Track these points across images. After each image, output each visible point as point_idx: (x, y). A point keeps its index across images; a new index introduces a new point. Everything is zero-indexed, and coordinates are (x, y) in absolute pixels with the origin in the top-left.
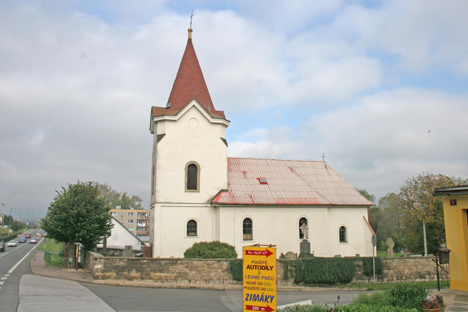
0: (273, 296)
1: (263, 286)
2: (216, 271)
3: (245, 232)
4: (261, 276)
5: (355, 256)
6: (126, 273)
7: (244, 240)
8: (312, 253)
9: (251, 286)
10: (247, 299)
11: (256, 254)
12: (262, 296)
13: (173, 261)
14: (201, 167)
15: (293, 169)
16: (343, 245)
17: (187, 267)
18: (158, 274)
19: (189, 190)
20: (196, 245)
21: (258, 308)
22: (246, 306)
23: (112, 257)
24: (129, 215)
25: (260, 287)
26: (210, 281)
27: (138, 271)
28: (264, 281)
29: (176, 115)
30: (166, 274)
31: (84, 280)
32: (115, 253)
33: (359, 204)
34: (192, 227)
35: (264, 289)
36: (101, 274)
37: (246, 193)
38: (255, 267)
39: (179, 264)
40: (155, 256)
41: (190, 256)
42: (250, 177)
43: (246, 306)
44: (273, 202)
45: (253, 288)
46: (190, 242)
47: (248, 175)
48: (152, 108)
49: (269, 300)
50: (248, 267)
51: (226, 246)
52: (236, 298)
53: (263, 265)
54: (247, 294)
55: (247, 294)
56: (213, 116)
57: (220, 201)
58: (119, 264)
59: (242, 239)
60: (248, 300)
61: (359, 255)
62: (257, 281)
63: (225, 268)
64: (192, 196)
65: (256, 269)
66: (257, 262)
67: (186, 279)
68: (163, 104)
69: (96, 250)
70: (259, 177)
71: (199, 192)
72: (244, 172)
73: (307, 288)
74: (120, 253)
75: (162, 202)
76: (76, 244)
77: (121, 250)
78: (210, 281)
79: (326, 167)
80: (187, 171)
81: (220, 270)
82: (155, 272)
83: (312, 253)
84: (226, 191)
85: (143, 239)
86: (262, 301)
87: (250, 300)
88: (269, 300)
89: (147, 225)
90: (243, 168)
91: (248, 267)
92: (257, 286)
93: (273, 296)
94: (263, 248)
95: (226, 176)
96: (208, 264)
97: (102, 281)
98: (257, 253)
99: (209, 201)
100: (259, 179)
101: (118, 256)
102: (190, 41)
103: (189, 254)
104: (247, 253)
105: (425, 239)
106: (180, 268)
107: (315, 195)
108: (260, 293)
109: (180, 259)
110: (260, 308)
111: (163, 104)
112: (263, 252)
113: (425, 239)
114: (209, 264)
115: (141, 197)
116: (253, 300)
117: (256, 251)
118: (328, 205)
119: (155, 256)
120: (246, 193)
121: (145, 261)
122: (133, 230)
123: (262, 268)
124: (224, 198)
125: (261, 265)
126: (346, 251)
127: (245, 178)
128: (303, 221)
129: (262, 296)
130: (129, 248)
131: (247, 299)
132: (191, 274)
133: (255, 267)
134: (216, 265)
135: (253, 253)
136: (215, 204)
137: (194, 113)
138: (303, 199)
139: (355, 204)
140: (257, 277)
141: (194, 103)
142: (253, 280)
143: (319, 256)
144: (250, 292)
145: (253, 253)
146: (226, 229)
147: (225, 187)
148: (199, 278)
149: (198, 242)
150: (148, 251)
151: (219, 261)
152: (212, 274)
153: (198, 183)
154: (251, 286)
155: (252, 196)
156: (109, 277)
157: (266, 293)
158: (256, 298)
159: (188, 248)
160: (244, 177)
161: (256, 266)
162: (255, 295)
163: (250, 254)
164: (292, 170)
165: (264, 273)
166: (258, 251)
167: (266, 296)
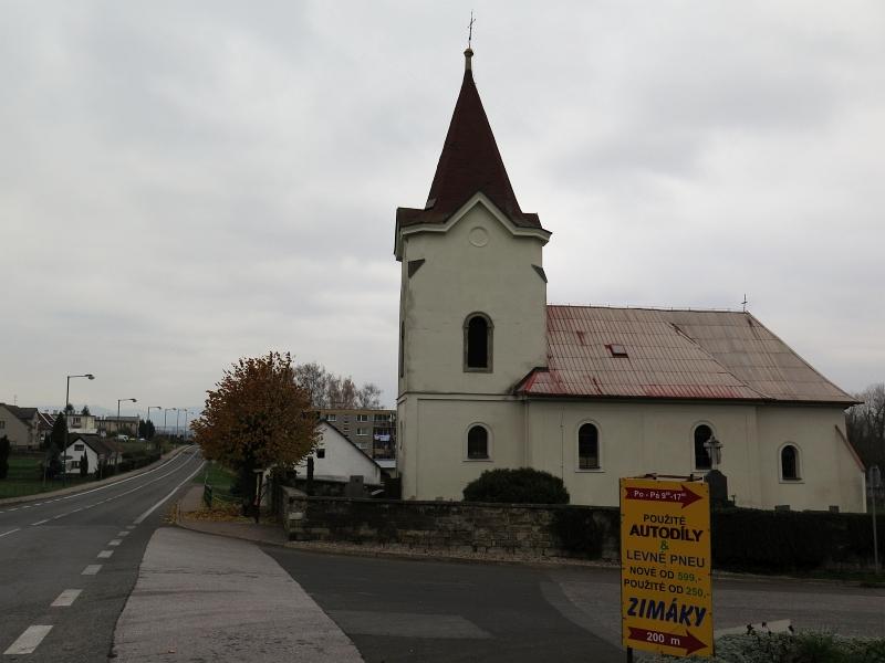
0: (704, 610)
1: (676, 582)
2: (527, 529)
3: (583, 452)
4: (668, 553)
5: (828, 509)
6: (349, 530)
7: (581, 467)
8: (730, 498)
9: (642, 578)
10: (631, 613)
11: (654, 498)
12: (674, 606)
13: (441, 508)
17: (470, 520)
18: (412, 532)
20: (486, 475)
21: (661, 638)
22: (631, 629)
23: (324, 498)
24: (359, 419)
25: (667, 582)
26: (516, 549)
27: (371, 526)
28: (676, 567)
29: (445, 222)
30: (427, 533)
31: (270, 542)
32: (333, 490)
34: (478, 441)
35: (678, 589)
36: (300, 530)
37: (585, 374)
38: (651, 530)
39: (454, 513)
40: (406, 496)
41: (649, 484)
42: (592, 344)
43: (631, 629)
44: (639, 392)
45: (647, 585)
46: (475, 471)
47: (588, 339)
48: (399, 210)
49: (693, 617)
50: (634, 530)
51: (546, 477)
52: (590, 601)
53: (674, 526)
54: (632, 600)
55: (632, 600)
56: (517, 222)
57: (535, 388)
58: (335, 511)
60: (634, 614)
61: (837, 508)
62: (659, 566)
63: (547, 523)
65: (655, 535)
66: (657, 519)
67: (467, 543)
68: (419, 200)
69: (294, 484)
71: (491, 371)
72: (580, 334)
73: (723, 573)
74: (341, 489)
76: (256, 471)
77: (342, 485)
78: (516, 549)
79: (750, 322)
81: (536, 529)
82: (407, 528)
83: (730, 498)
84: (545, 370)
85: (384, 464)
86: (672, 619)
87: (641, 615)
88: (693, 617)
89: (391, 438)
90: (577, 326)
91: (634, 530)
92: (658, 579)
93: (704, 610)
94: (676, 484)
95: (544, 341)
96: (512, 515)
97: (302, 545)
98: (658, 496)
99: (511, 389)
100: (609, 347)
101: (336, 495)
103: (476, 492)
104: (630, 493)
105: (153, 509)
106: (456, 520)
107: (727, 379)
108: (666, 597)
109: (455, 504)
110: (668, 637)
111: (419, 200)
112: (673, 492)
113: (153, 509)
114: (514, 514)
115: (378, 386)
116: (648, 616)
117: (655, 491)
118: (758, 400)
119: (406, 496)
120: (585, 374)
121: (387, 506)
122: (368, 447)
123: (670, 534)
124: (541, 385)
125: (669, 527)
126: (798, 499)
127: (582, 345)
128: (703, 434)
129: (674, 606)
130: (357, 479)
131: (631, 613)
132: (477, 533)
133: (651, 530)
134: (528, 517)
135: (646, 494)
136: (521, 394)
137: (479, 219)
139: (814, 399)
140: (658, 558)
141: (479, 198)
142: (648, 565)
144: (640, 594)
145: (646, 494)
146: (547, 447)
147: (542, 364)
148: (494, 543)
149: (491, 470)
150: (392, 483)
151: (534, 509)
152: (521, 536)
153: (488, 354)
154: (642, 578)
156: (315, 538)
157: (683, 600)
158: (655, 610)
159: (472, 480)
161: (655, 528)
162: (652, 603)
163: (638, 497)
164: (677, 329)
165: (677, 547)
166: (660, 492)
167: (684, 607)
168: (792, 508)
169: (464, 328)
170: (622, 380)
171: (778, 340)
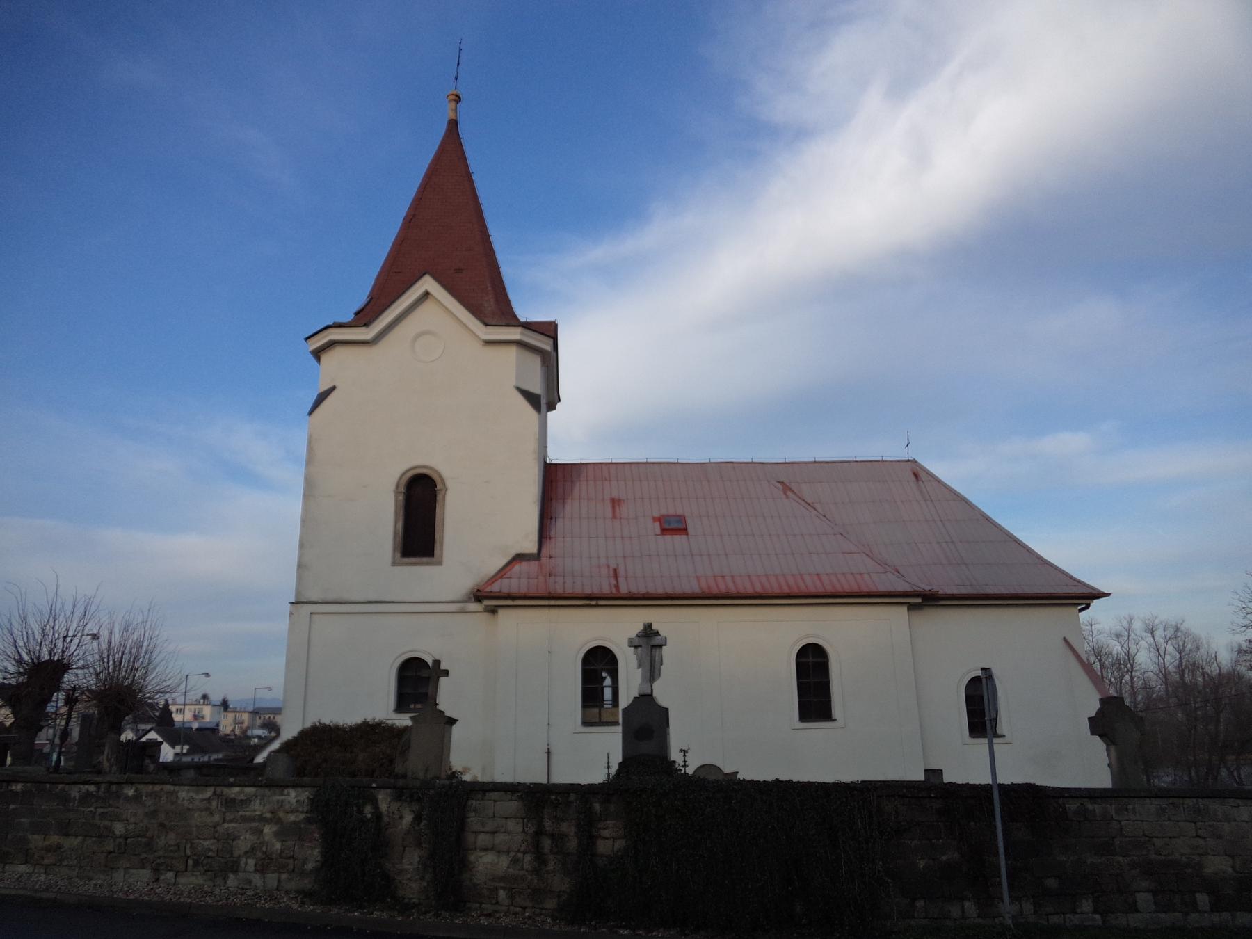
5: (920, 777)
7: (586, 723)
14: (449, 484)
15: (793, 486)
16: (817, 730)
19: (406, 560)
33: (1012, 591)
56: (487, 320)
59: (579, 720)
61: (939, 772)
64: (420, 579)
70: (664, 512)
71: (440, 563)
72: (615, 502)
75: (314, 598)
80: (401, 498)
102: (453, 125)
114: (233, 800)
127: (614, 517)
136: (488, 598)
138: (807, 578)
139: (1019, 591)
141: (427, 283)
143: (1083, 786)
153: (437, 536)
155: (621, 573)
160: (610, 515)
164: (786, 488)
168: (740, 776)
169: (397, 492)
170: (668, 564)
171: (963, 500)
